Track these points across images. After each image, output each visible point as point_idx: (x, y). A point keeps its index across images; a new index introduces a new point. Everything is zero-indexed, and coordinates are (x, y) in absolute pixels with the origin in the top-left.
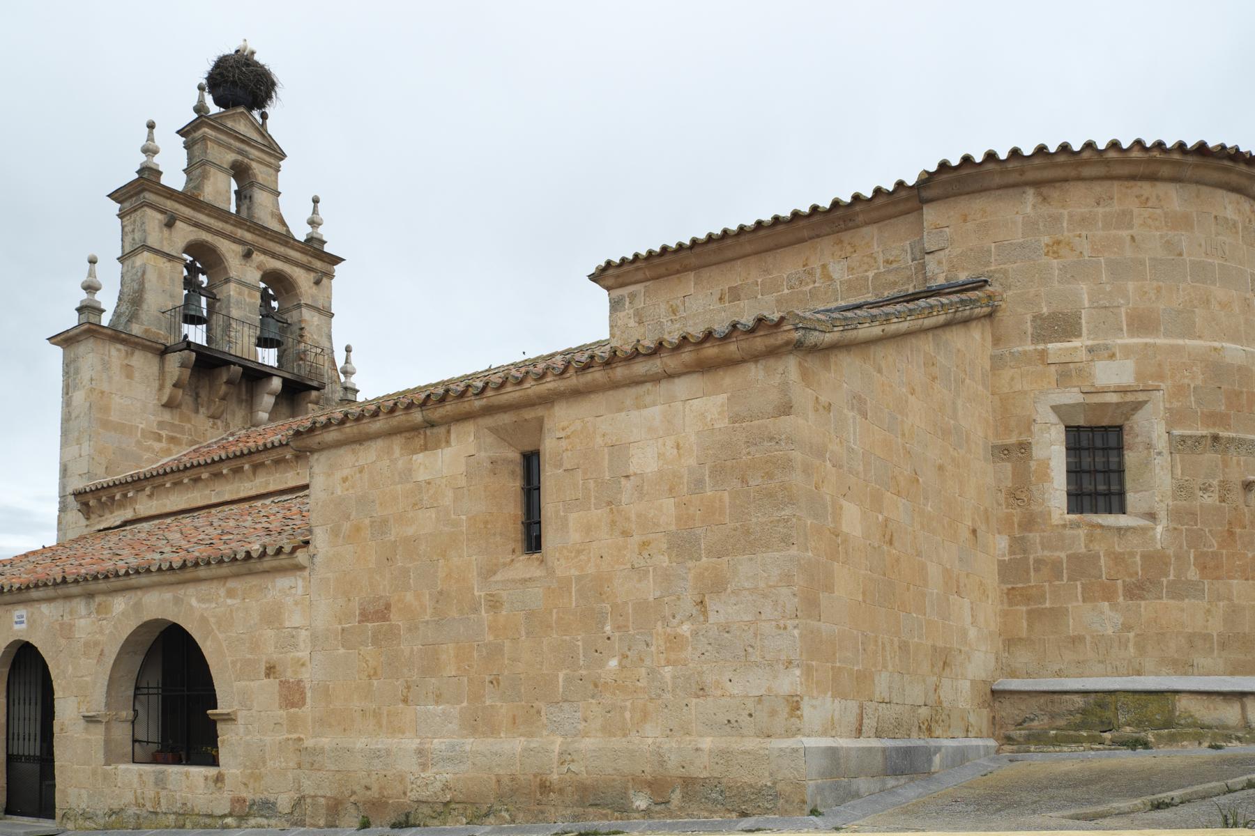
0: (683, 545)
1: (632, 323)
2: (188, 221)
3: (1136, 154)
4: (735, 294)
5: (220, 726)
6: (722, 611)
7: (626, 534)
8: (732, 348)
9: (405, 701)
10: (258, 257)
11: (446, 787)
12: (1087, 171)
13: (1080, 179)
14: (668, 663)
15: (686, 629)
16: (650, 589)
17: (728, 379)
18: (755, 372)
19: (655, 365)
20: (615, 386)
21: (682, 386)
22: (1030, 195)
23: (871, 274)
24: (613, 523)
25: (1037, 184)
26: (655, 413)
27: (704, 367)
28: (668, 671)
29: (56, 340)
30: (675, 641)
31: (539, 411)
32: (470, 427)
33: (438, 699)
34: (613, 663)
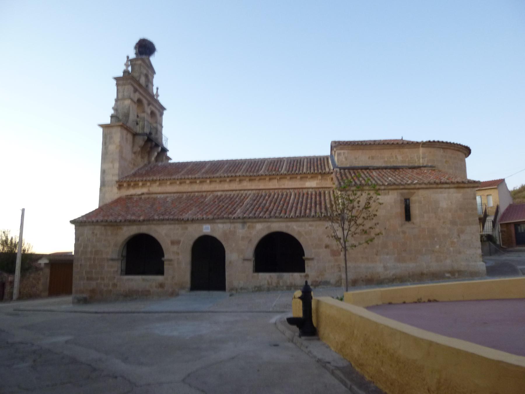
0: (454, 223)
1: (344, 160)
2: (140, 93)
3: (456, 146)
4: (373, 158)
5: (306, 262)
6: (463, 237)
7: (439, 220)
8: (466, 185)
9: (377, 255)
10: (151, 106)
11: (393, 275)
12: (452, 148)
13: (450, 149)
14: (451, 247)
15: (455, 240)
16: (446, 232)
17: (462, 191)
18: (468, 190)
19: (448, 186)
20: (437, 188)
21: (452, 190)
22: (442, 150)
23: (407, 160)
24: (436, 217)
25: (443, 148)
26: (445, 195)
27: (458, 188)
28: (451, 249)
29: (102, 126)
30: (453, 243)
31: (415, 191)
32: (395, 192)
33: (387, 254)
34: (438, 247)
